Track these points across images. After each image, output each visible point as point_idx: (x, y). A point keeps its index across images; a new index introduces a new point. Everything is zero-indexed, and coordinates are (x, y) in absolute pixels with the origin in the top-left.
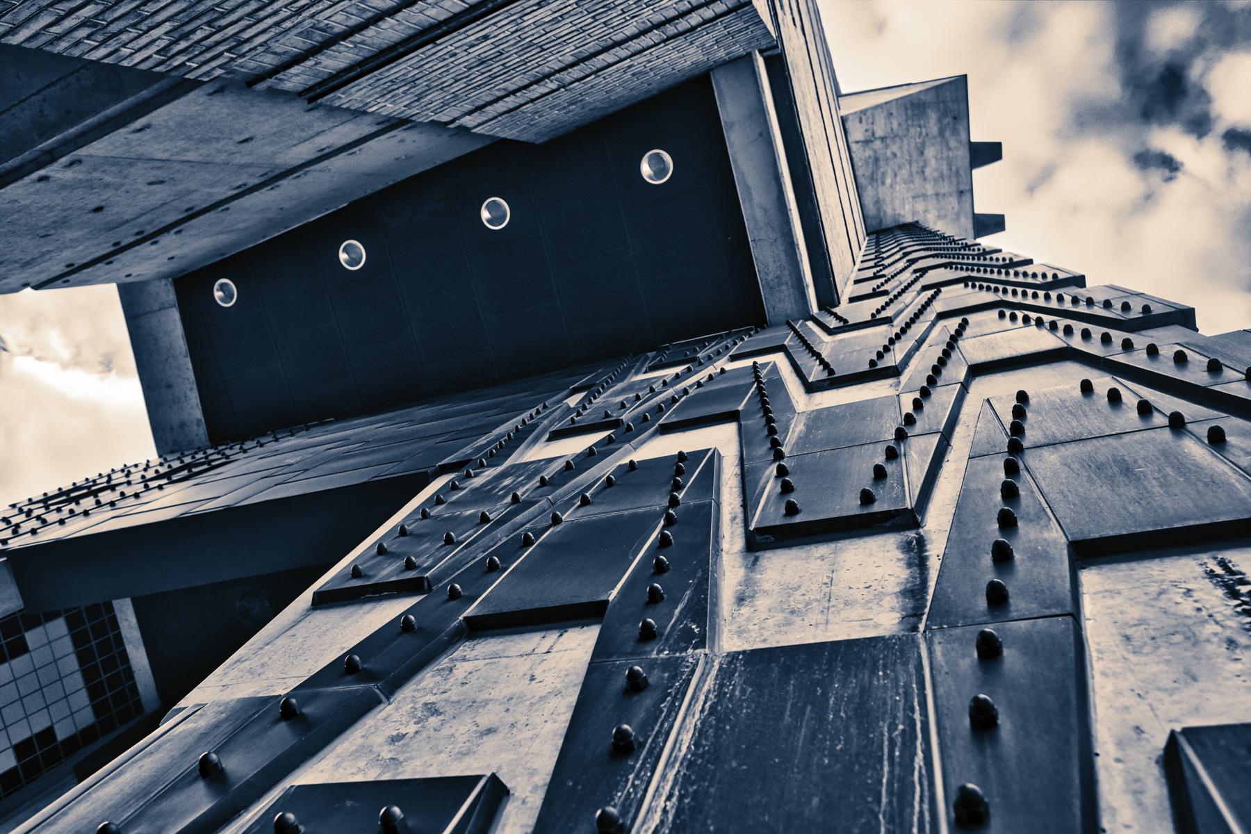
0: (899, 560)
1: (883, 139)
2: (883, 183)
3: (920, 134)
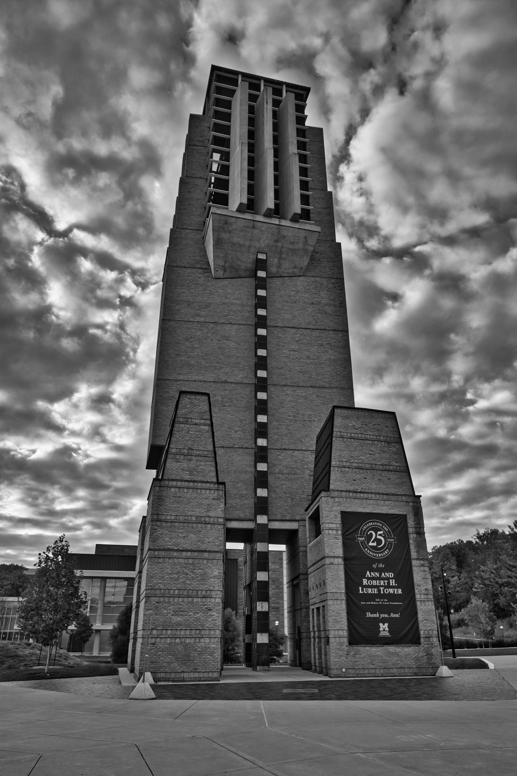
0: (355, 148)
1: (225, 262)
2: (240, 266)
3: (227, 243)
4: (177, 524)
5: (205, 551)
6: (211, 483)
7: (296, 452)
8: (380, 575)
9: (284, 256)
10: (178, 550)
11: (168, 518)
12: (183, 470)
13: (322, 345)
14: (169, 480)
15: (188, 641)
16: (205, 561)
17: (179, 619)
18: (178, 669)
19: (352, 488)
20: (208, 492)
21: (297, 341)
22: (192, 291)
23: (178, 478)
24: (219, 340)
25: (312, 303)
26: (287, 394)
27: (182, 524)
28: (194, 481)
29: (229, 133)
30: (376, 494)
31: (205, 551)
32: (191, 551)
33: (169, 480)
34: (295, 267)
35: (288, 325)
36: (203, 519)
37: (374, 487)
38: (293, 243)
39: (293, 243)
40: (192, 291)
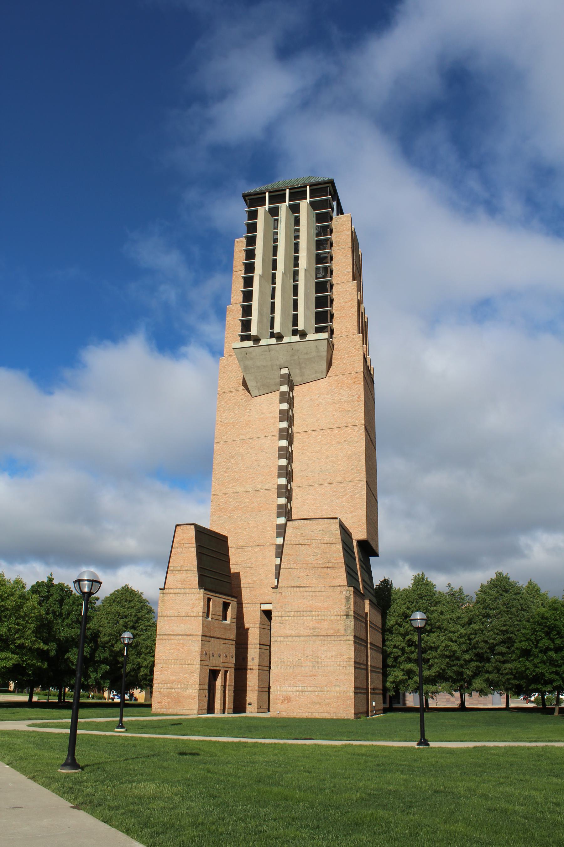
1: (257, 383)
2: (269, 383)
4: (173, 618)
5: (190, 635)
6: (195, 588)
9: (303, 365)
10: (174, 635)
11: (168, 614)
13: (340, 442)
14: (169, 589)
15: (179, 691)
16: (190, 641)
17: (174, 677)
19: (296, 584)
20: (193, 595)
21: (319, 442)
22: (236, 412)
23: (174, 587)
24: (256, 453)
25: (333, 403)
26: (309, 494)
27: (176, 618)
28: (184, 588)
30: (315, 587)
31: (190, 635)
32: (182, 635)
33: (169, 589)
34: (316, 372)
35: (311, 429)
36: (189, 614)
37: (314, 582)
38: (307, 354)
39: (307, 354)
40: (236, 412)
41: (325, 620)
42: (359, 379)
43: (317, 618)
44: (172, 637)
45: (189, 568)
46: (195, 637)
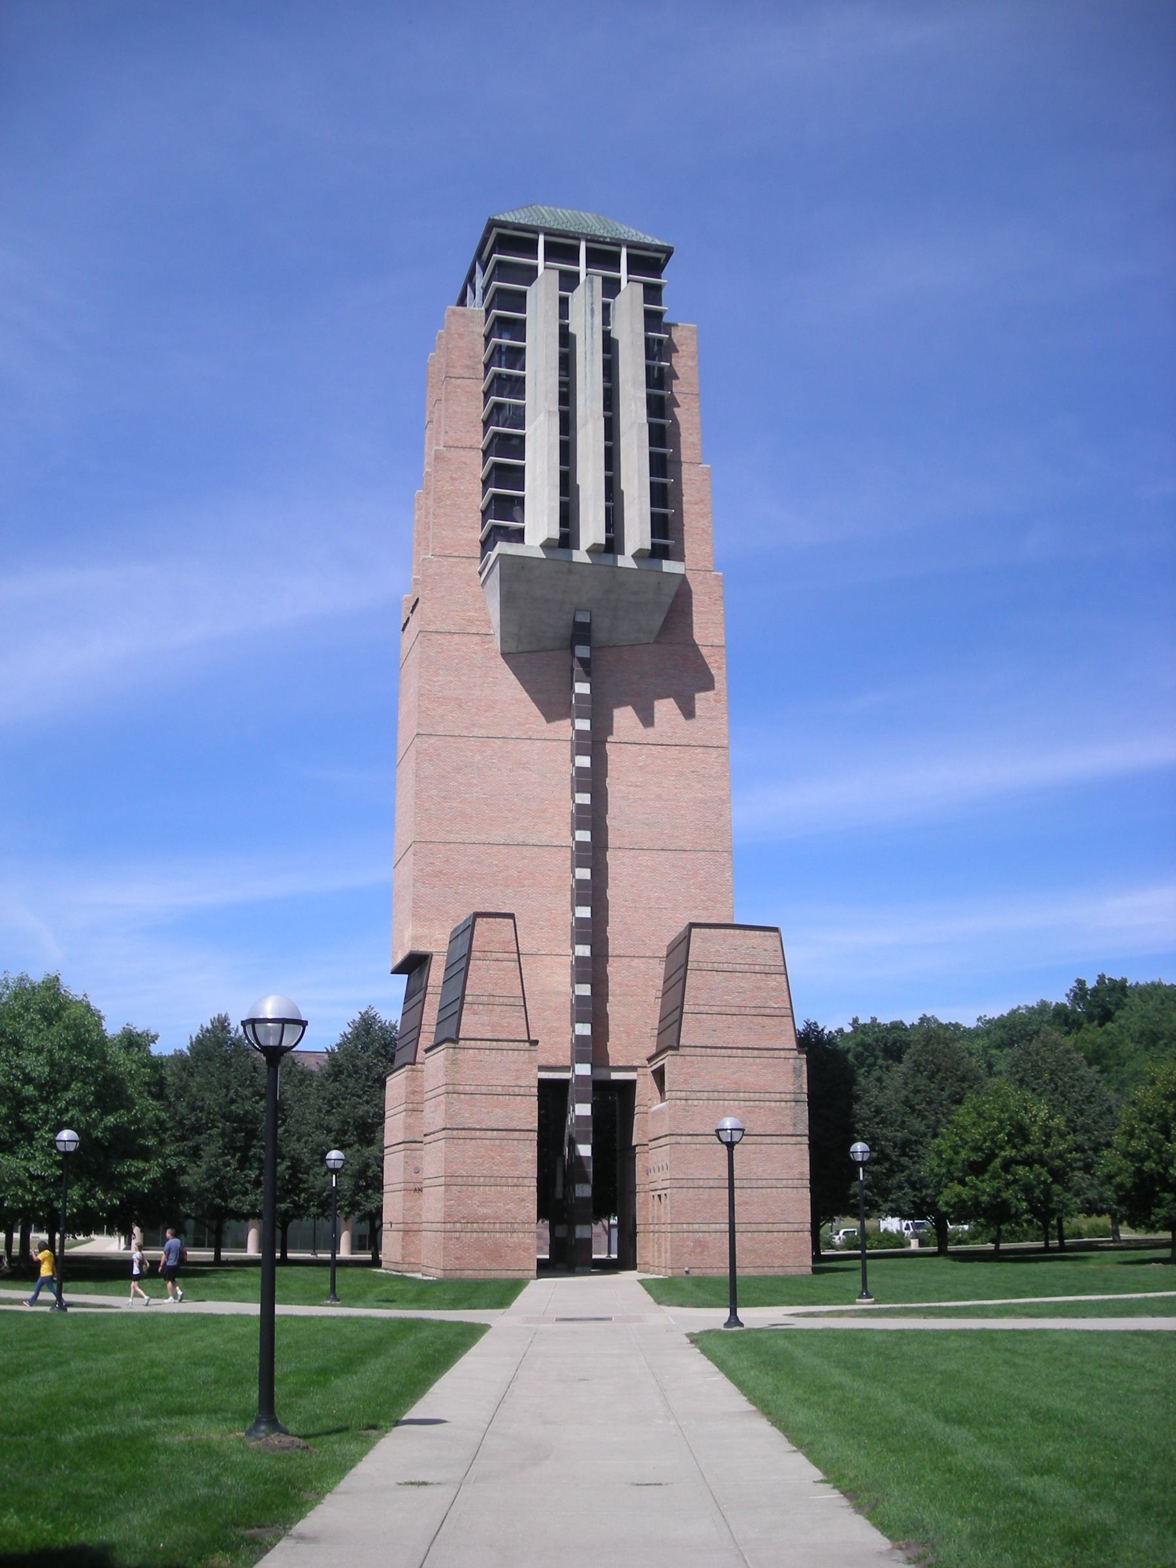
7: (636, 960)
8: (1053, 1227)
12: (483, 1025)
13: (682, 774)
15: (498, 1235)
17: (485, 1211)
18: (488, 1266)
21: (641, 768)
22: (464, 679)
24: (511, 770)
26: (623, 864)
29: (523, 309)
35: (626, 740)
40: (464, 679)
41: (761, 1108)
42: (718, 658)
43: (747, 1103)
44: (478, 1133)
45: (506, 1000)
46: (523, 1135)
